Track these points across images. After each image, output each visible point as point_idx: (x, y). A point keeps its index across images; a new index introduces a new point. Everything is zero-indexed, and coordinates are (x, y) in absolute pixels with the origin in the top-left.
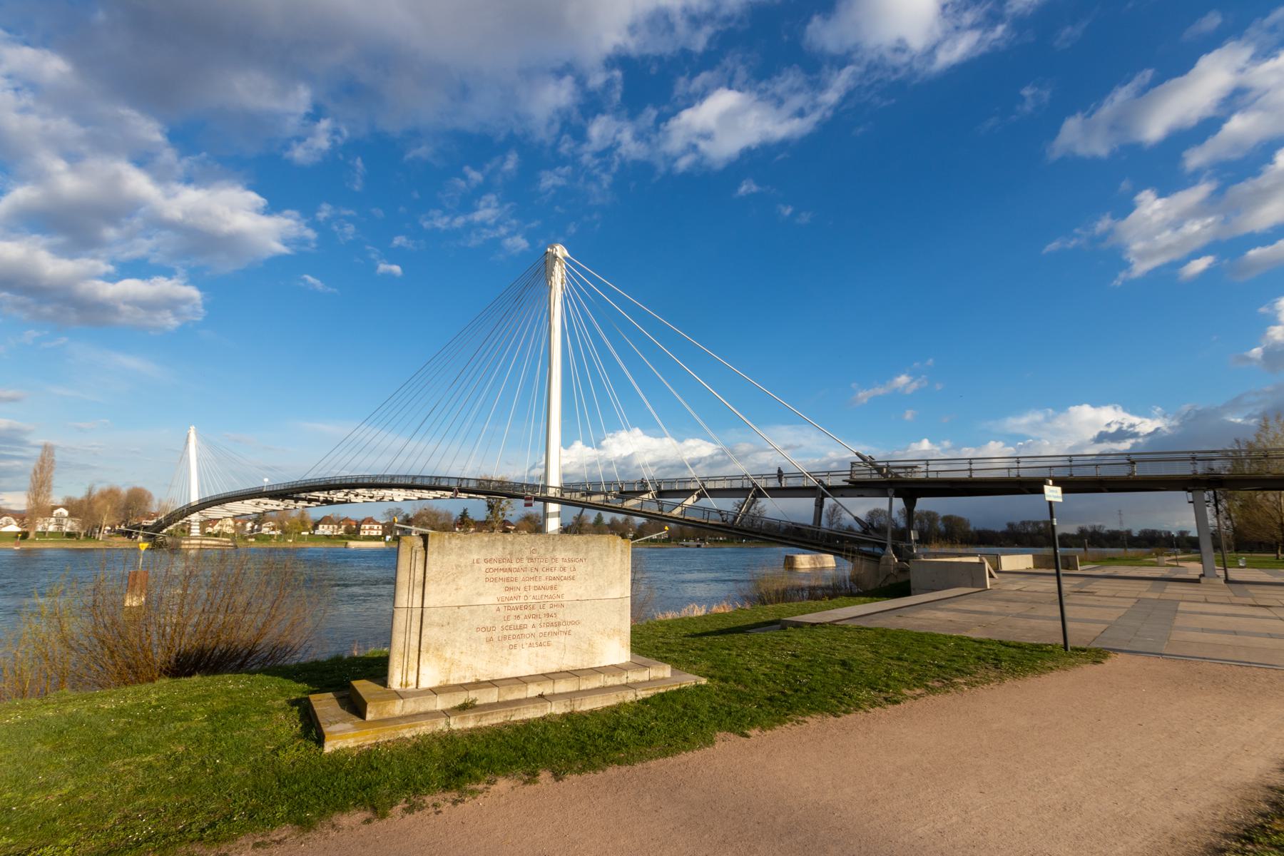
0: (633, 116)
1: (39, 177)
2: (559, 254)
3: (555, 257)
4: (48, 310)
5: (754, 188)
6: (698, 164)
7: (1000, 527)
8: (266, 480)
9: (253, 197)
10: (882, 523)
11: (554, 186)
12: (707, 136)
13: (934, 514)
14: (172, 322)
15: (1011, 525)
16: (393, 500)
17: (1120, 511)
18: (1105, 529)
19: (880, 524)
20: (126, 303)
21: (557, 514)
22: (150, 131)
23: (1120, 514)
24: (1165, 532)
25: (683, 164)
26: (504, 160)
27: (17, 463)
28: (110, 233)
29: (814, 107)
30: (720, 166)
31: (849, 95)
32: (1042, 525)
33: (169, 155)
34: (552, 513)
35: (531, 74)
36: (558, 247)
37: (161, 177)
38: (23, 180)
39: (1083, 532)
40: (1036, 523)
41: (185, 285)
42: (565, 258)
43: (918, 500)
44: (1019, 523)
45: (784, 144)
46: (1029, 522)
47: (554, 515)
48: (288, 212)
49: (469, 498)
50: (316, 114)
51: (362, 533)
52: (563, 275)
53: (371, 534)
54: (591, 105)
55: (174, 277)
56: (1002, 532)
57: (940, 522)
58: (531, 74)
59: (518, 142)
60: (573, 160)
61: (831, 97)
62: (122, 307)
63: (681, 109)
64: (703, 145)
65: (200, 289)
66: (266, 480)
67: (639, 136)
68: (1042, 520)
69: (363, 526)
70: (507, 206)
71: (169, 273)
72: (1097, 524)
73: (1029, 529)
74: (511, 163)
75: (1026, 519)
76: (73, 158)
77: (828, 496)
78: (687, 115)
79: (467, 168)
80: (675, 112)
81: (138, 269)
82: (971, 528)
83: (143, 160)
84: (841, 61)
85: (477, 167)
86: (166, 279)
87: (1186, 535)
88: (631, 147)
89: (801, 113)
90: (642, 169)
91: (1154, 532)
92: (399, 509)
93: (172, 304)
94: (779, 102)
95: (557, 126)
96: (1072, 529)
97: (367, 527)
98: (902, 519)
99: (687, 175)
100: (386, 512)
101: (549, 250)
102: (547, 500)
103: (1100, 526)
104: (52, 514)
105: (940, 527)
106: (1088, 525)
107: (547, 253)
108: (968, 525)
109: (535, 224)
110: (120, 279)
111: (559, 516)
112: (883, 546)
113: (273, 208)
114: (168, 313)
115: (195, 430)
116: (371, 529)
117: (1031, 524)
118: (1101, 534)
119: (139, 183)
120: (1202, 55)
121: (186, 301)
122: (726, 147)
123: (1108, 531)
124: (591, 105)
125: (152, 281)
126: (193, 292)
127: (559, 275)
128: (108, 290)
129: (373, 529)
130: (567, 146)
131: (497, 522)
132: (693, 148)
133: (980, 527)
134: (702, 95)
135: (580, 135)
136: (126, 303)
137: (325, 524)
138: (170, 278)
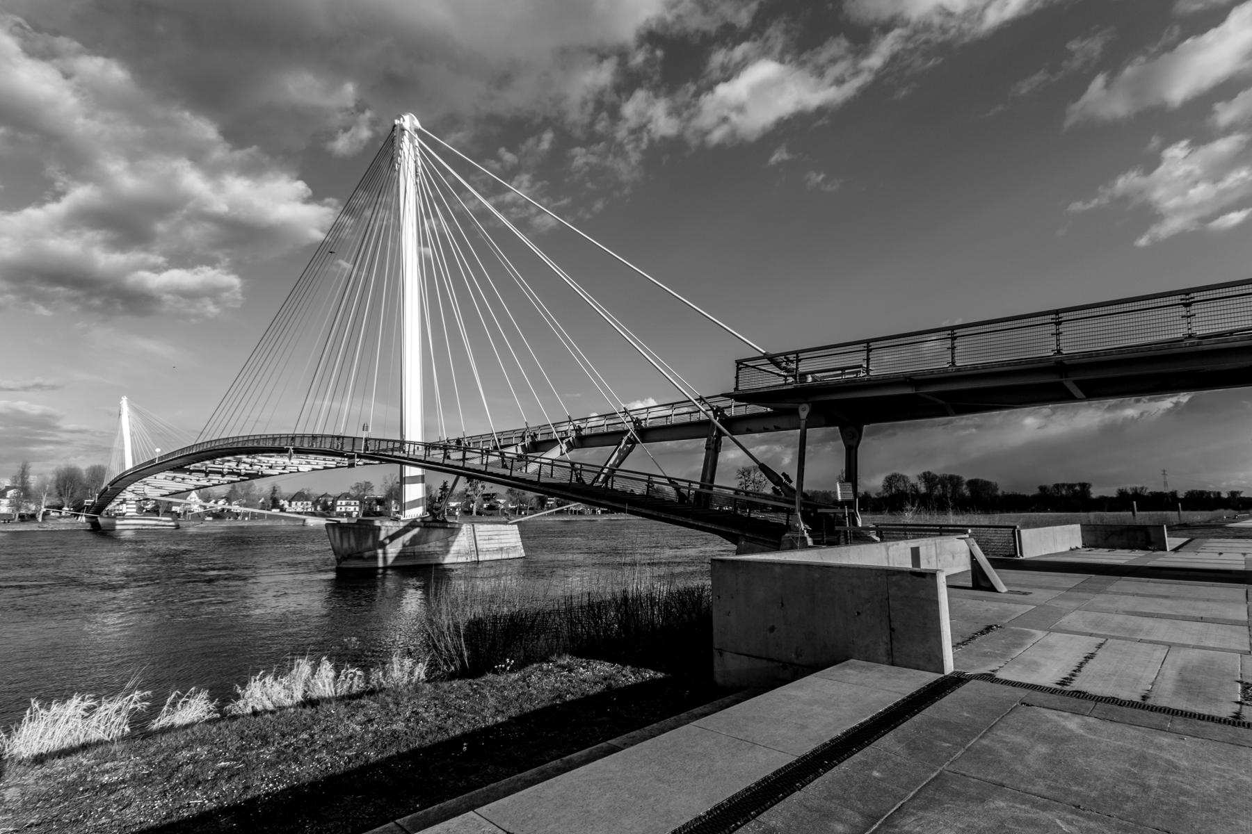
0: (671, 92)
1: (97, 178)
2: (407, 125)
3: (403, 130)
4: (97, 302)
5: (785, 156)
6: (733, 134)
7: (1032, 491)
8: (158, 450)
9: (300, 186)
10: (901, 489)
11: (587, 164)
12: (740, 109)
13: (959, 478)
14: (212, 309)
15: (1042, 489)
16: (298, 471)
17: (1164, 471)
18: (1148, 491)
19: (898, 490)
20: (169, 293)
21: (420, 478)
22: (205, 130)
23: (1164, 474)
24: (1214, 493)
25: (717, 136)
26: (540, 141)
27: (50, 447)
28: (160, 227)
29: (856, 73)
30: (752, 138)
31: (894, 58)
32: (1077, 488)
33: (220, 152)
34: (410, 477)
35: (567, 57)
36: (407, 117)
37: (213, 171)
38: (85, 180)
39: (1122, 494)
40: (1071, 486)
41: (228, 274)
42: (418, 131)
43: (837, 428)
44: (1052, 486)
45: (821, 111)
46: (1063, 485)
47: (414, 480)
48: (327, 200)
49: (365, 464)
50: (360, 108)
51: (338, 509)
52: (416, 155)
53: (348, 510)
54: (628, 82)
55: (217, 265)
56: (1034, 497)
57: (964, 486)
58: (567, 57)
59: (555, 122)
60: (608, 138)
61: (875, 61)
62: (165, 297)
63: (717, 83)
64: (734, 117)
65: (241, 276)
66: (158, 450)
67: (674, 112)
68: (1077, 482)
69: (339, 503)
70: (539, 185)
71: (212, 262)
72: (1139, 486)
73: (1064, 492)
74: (547, 139)
75: (1060, 481)
76: (134, 156)
77: (725, 435)
78: (722, 90)
79: (502, 150)
80: (710, 88)
81: (182, 259)
82: (999, 493)
83: (197, 155)
84: (886, 28)
85: (512, 149)
86: (209, 268)
87: (1238, 496)
88: (663, 123)
89: (840, 81)
90: (675, 144)
91: (1202, 493)
92: (368, 483)
93: (213, 293)
94: (820, 72)
95: (590, 107)
96: (1112, 492)
97: (344, 502)
98: (923, 484)
99: (720, 147)
100: (354, 486)
101: (397, 122)
102: (403, 462)
103: (1142, 488)
104: (6, 495)
105: (965, 491)
106: (1129, 487)
107: (395, 126)
108: (996, 489)
109: (564, 202)
110: (166, 269)
111: (423, 482)
112: (790, 512)
113: (316, 197)
114: (207, 301)
115: (128, 401)
116: (347, 505)
117: (1066, 487)
118: (1143, 496)
119: (193, 181)
120: (1239, 92)
121: (229, 288)
122: (760, 118)
123: (1151, 493)
124: (628, 82)
125: (196, 270)
126: (234, 280)
127: (409, 154)
128: (154, 281)
129: (350, 505)
130: (603, 123)
131: (476, 495)
132: (725, 120)
133: (1009, 491)
134: (743, 65)
135: (615, 115)
136: (169, 293)
137: (299, 501)
138: (214, 268)
